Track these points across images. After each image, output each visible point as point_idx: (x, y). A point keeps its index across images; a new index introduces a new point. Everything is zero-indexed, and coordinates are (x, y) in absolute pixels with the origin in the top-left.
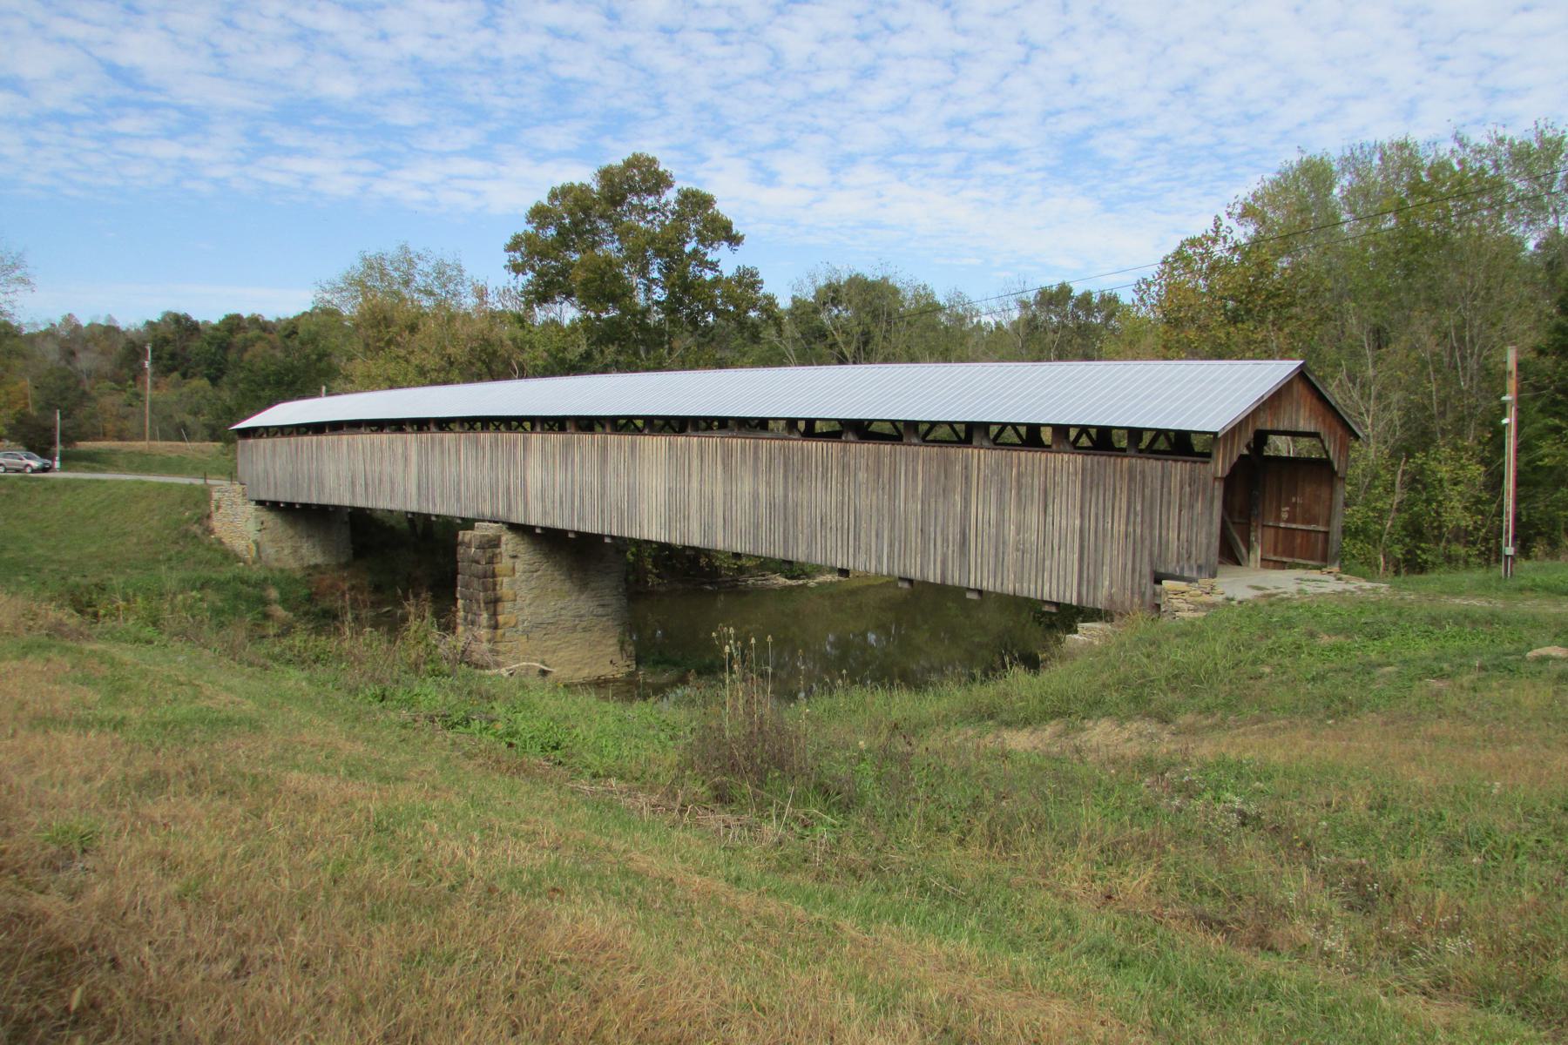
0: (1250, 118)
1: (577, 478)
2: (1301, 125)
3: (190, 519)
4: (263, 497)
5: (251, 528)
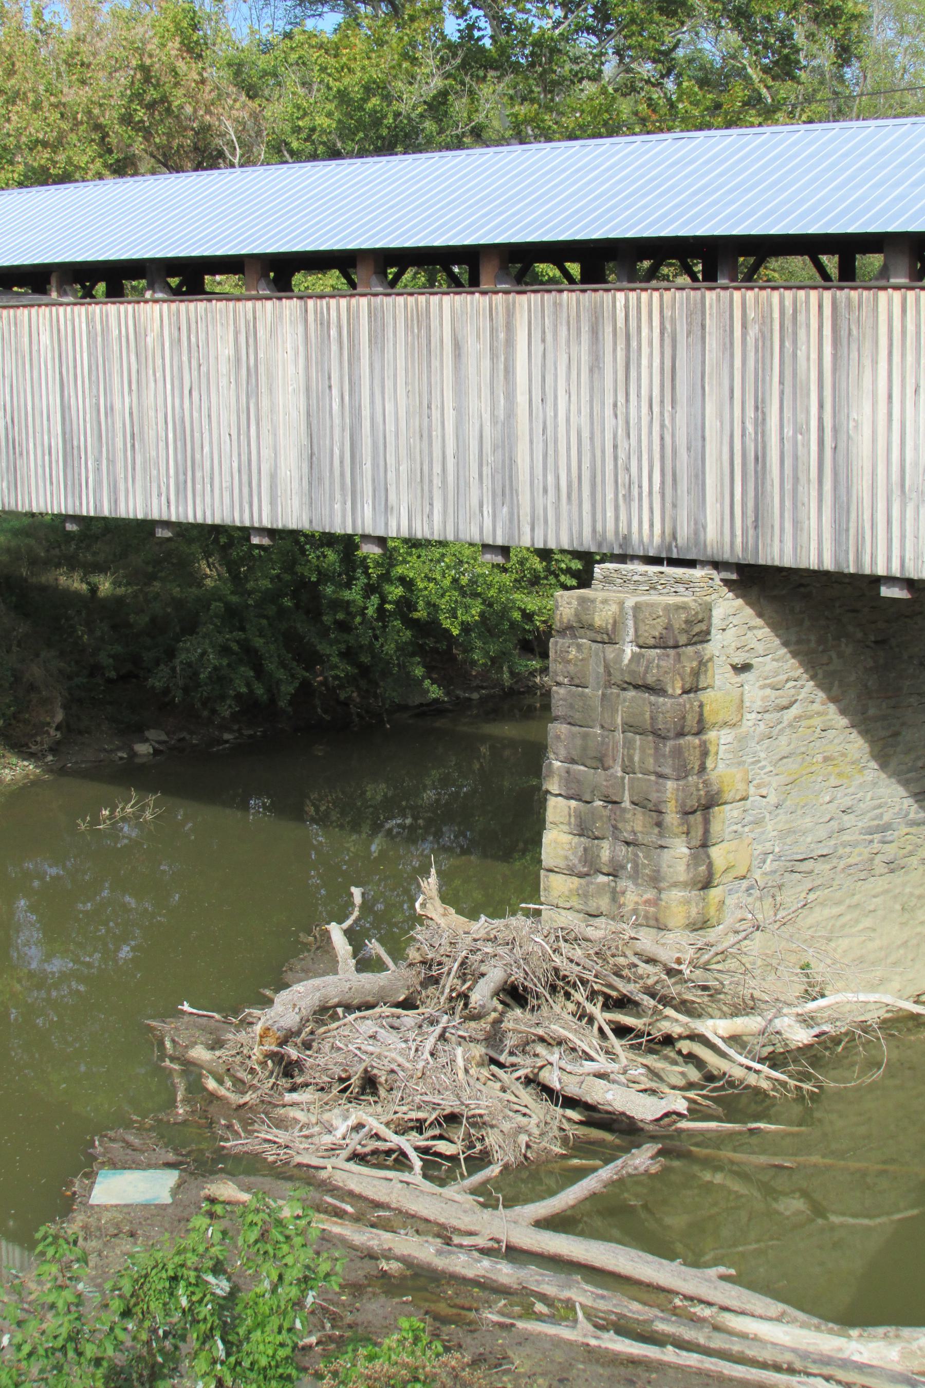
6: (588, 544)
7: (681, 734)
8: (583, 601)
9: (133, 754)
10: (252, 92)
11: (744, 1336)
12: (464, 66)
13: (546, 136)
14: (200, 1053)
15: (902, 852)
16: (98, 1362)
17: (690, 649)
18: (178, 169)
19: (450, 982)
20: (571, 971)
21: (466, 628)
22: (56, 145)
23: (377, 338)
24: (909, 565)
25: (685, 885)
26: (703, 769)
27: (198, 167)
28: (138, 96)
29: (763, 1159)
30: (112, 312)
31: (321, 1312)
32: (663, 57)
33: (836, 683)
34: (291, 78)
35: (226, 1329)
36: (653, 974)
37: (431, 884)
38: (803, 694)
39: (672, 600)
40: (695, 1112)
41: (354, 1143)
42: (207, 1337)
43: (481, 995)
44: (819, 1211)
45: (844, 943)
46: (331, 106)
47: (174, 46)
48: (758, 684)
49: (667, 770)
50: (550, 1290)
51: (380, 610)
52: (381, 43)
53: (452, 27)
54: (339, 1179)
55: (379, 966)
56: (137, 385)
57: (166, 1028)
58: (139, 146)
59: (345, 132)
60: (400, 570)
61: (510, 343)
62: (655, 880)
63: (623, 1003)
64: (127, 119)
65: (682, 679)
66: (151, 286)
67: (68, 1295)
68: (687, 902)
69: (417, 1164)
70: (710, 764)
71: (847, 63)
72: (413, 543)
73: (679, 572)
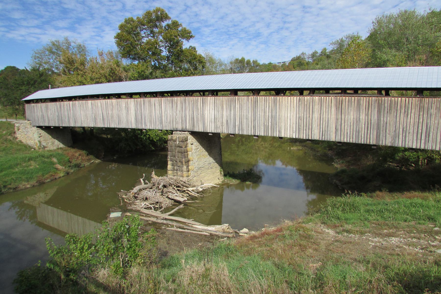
0: (235, 26)
1: (238, 114)
2: (246, 28)
3: (6, 134)
4: (42, 125)
5: (36, 136)
6: (172, 129)
7: (185, 153)
8: (172, 136)
9: (114, 158)
10: (126, 72)
11: (195, 228)
12: (154, 68)
13: (165, 77)
14: (124, 196)
16: (111, 238)
18: (117, 82)
19: (156, 185)
20: (172, 183)
21: (157, 140)
22: (100, 78)
23: (144, 104)
24: (212, 131)
25: (186, 172)
26: (187, 157)
27: (119, 81)
28: (111, 72)
29: (197, 205)
30: (71, 102)
31: (141, 229)
32: (180, 68)
34: (132, 70)
35: (128, 232)
36: (182, 183)
37: (154, 173)
39: (183, 136)
40: (188, 200)
41: (145, 206)
42: (126, 233)
43: (160, 187)
44: (204, 211)
45: (206, 178)
46: (137, 74)
47: (115, 65)
49: (183, 157)
50: (171, 223)
51: (146, 138)
52: (143, 65)
53: (153, 63)
54: (143, 211)
55: (147, 184)
56: (112, 110)
57: (119, 193)
58: (111, 79)
59: (139, 77)
60: (148, 133)
61: (161, 104)
62: (182, 171)
63: (179, 187)
64: (109, 75)
66: (113, 97)
67: (107, 230)
68: (186, 174)
69: (153, 209)
71: (204, 68)
72: (150, 130)
73: (184, 132)
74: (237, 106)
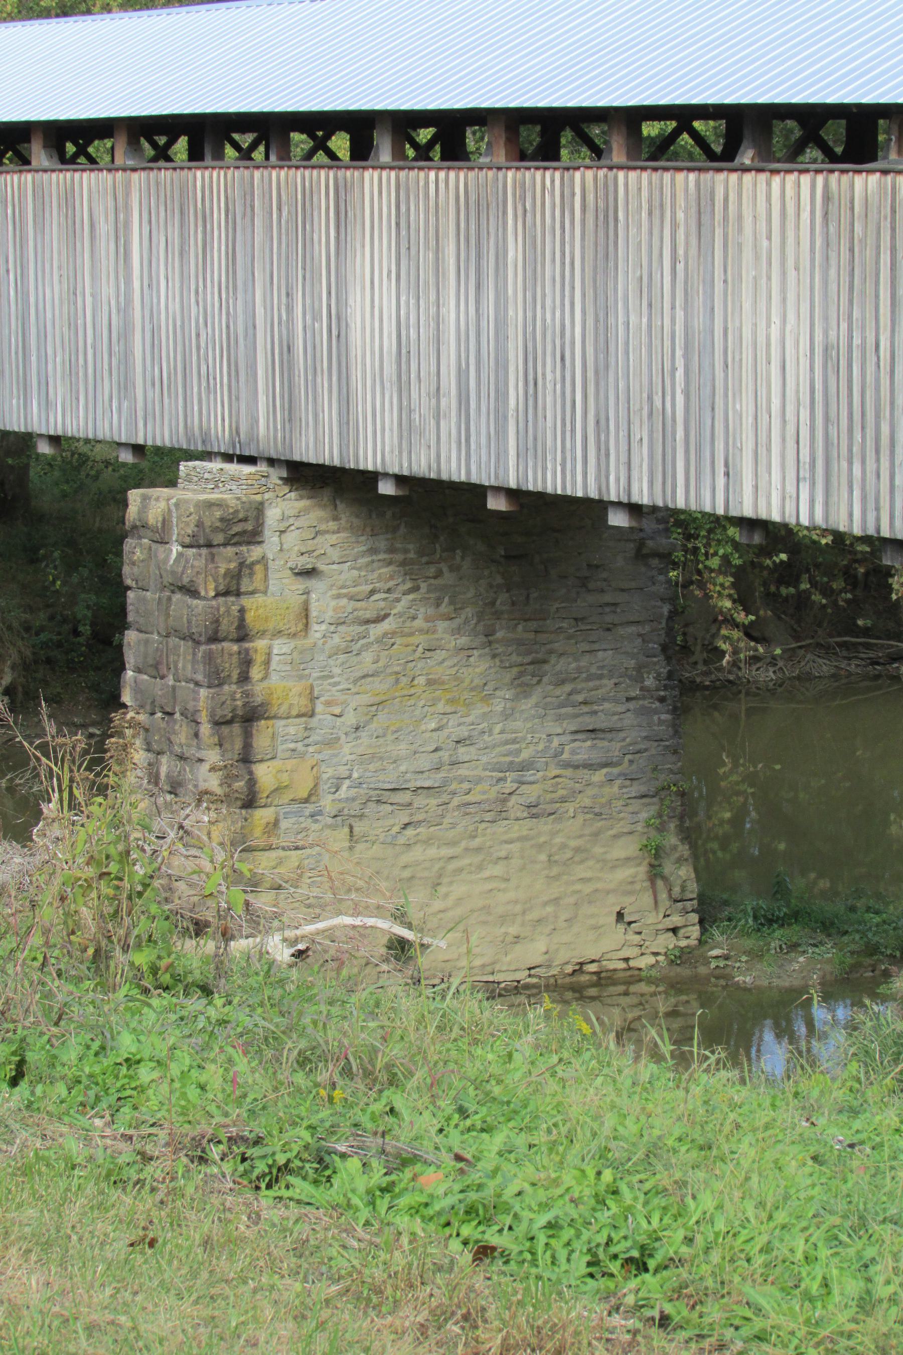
1: (515, 313)
15: (549, 796)
17: (230, 551)
33: (446, 599)
38: (399, 608)
48: (330, 593)
49: (199, 677)
65: (215, 581)
70: (255, 673)
74: (514, 252)
